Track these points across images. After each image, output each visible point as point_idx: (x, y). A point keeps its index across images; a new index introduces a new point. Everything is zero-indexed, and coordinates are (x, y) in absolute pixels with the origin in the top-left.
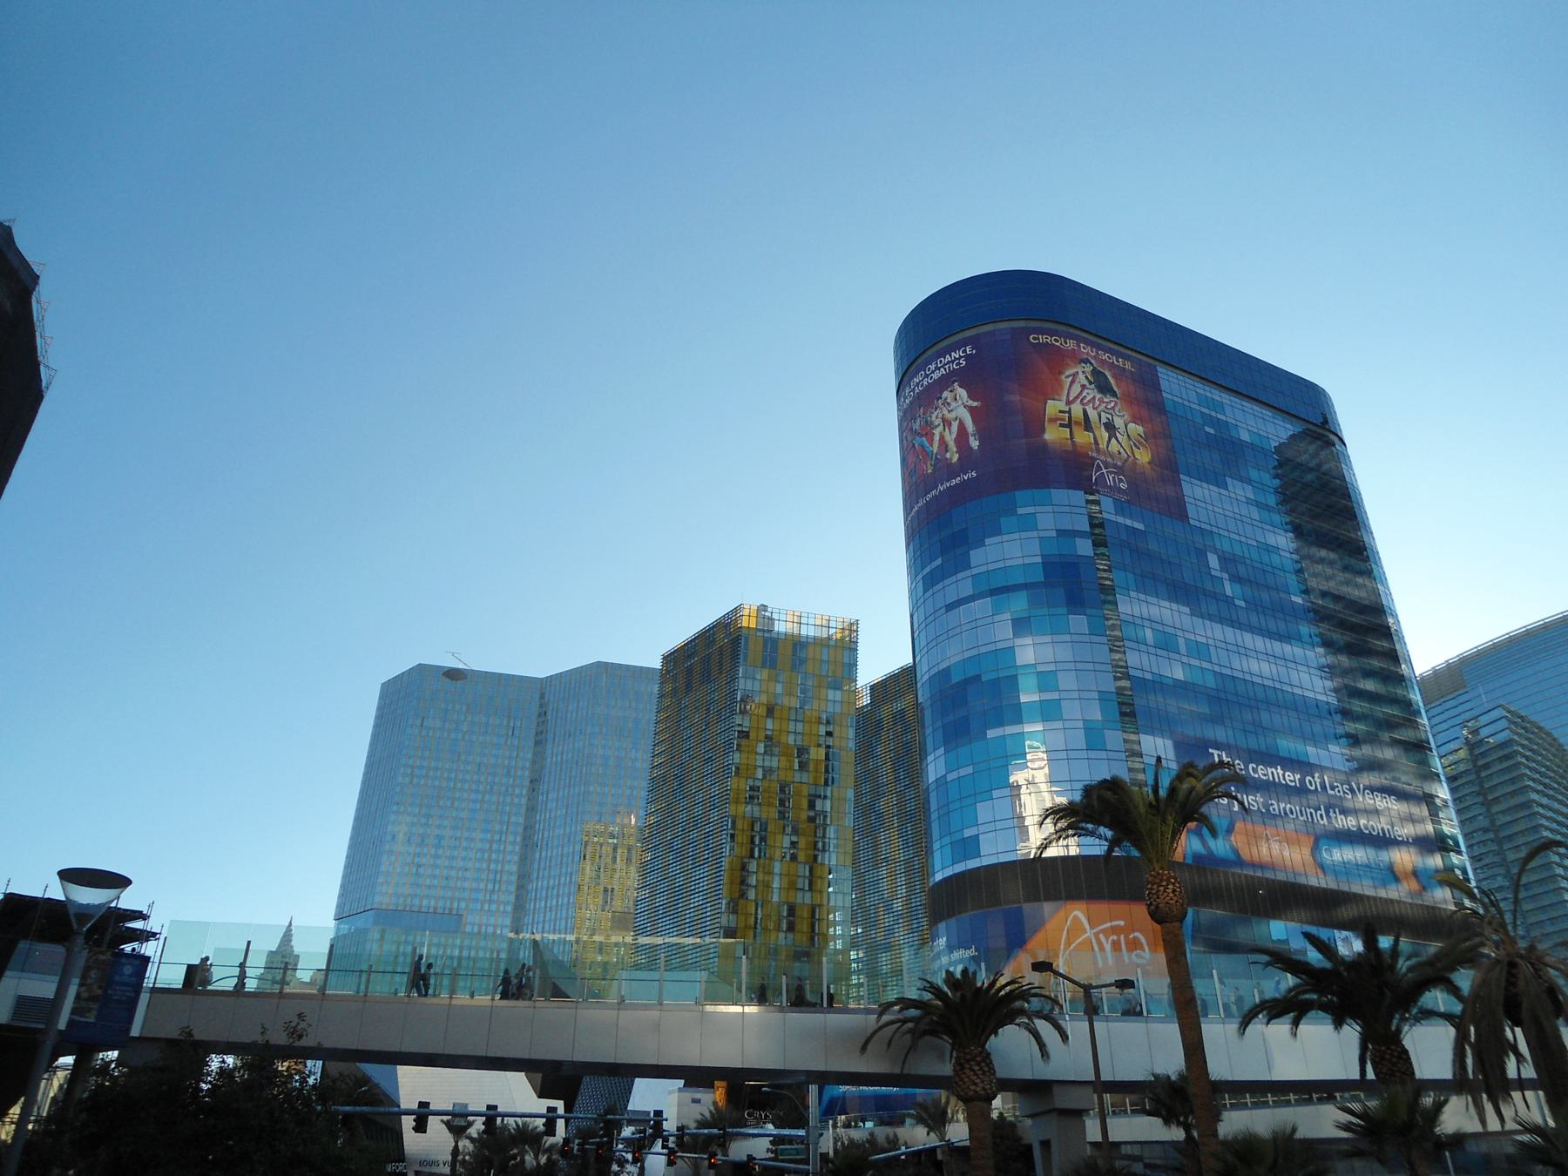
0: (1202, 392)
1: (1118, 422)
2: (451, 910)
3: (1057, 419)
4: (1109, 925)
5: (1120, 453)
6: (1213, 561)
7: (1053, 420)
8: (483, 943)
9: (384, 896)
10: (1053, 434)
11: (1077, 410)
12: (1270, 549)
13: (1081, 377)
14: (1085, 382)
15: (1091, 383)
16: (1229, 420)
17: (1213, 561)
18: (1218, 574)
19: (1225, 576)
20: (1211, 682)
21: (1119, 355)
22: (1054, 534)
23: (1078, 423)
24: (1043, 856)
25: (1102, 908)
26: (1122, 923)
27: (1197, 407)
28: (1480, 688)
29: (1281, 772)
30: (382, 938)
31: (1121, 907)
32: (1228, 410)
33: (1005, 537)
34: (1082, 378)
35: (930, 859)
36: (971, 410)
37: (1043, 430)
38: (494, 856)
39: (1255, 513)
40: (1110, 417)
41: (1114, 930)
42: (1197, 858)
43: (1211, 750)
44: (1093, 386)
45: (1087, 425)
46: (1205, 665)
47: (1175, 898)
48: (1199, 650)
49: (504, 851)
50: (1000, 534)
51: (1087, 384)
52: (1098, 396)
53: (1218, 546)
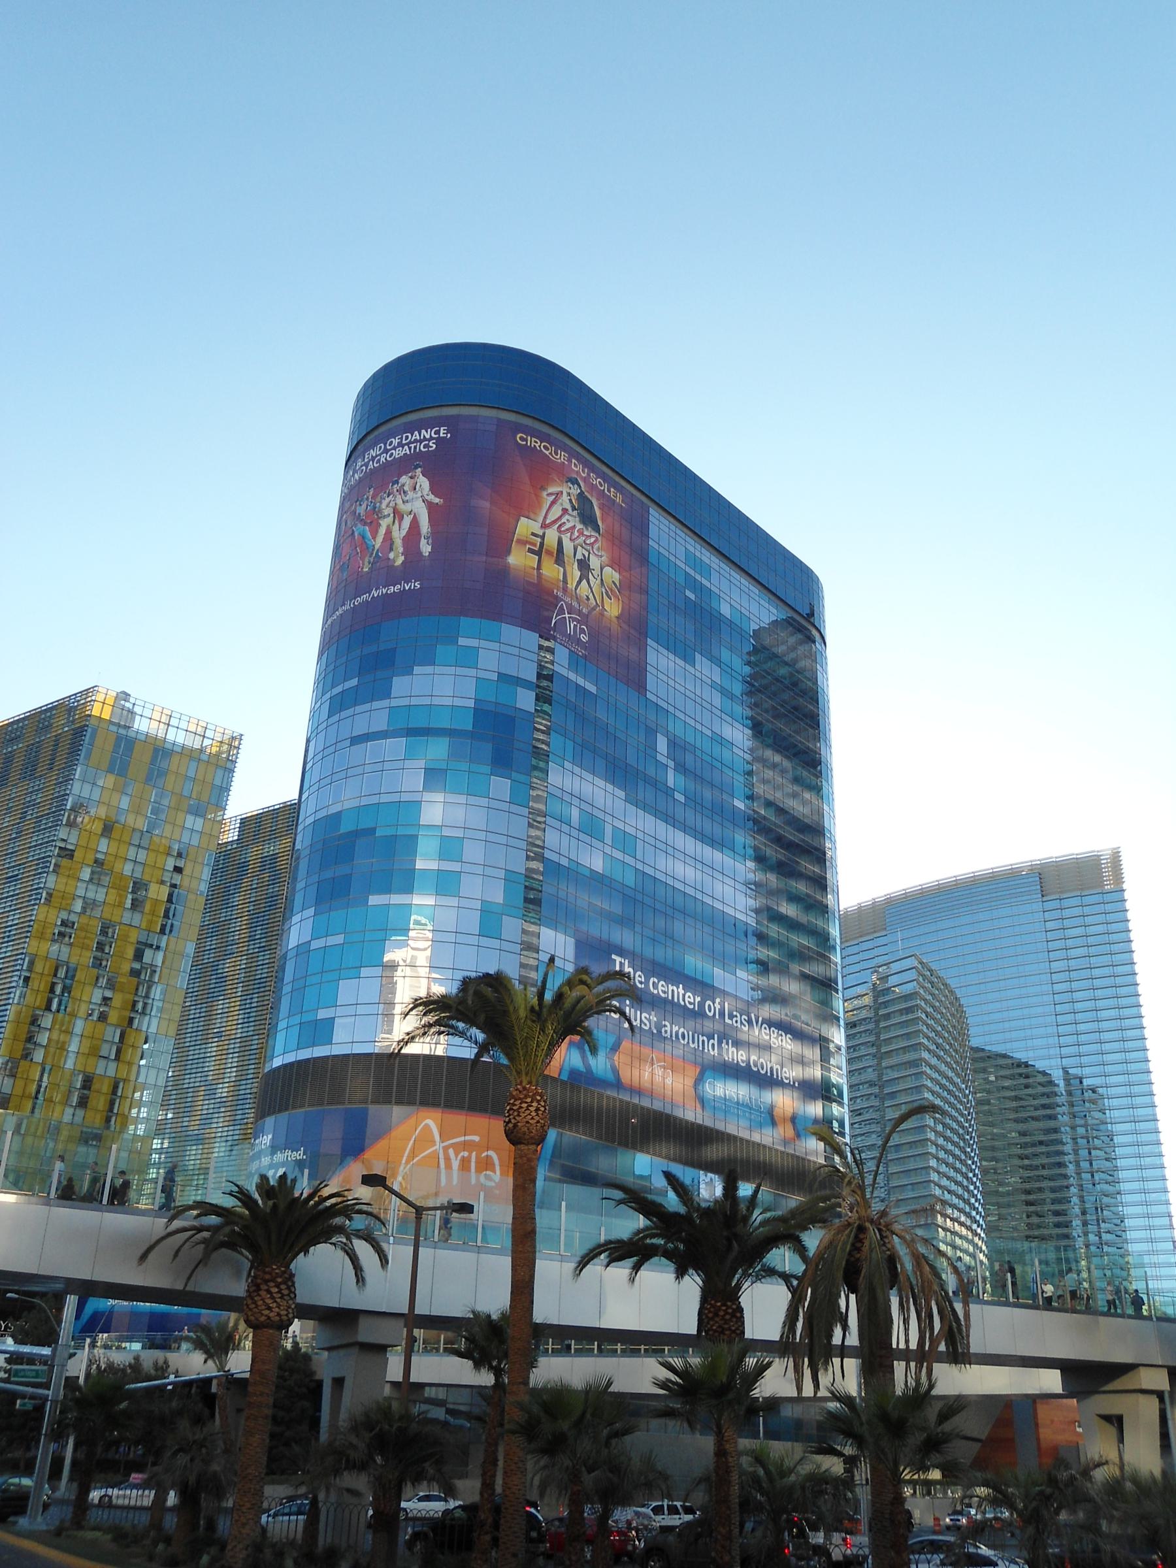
0: (692, 550)
1: (594, 563)
4: (462, 1139)
5: (588, 598)
6: (662, 744)
7: (522, 542)
10: (519, 559)
12: (721, 741)
13: (565, 498)
15: (574, 509)
16: (713, 588)
17: (662, 744)
18: (664, 760)
19: (671, 764)
20: (630, 880)
22: (495, 677)
25: (458, 1119)
26: (476, 1138)
27: (683, 566)
29: (681, 991)
32: (714, 576)
36: (430, 506)
37: (509, 552)
39: (717, 699)
40: (586, 554)
41: (466, 1145)
43: (614, 957)
44: (575, 513)
46: (629, 860)
47: (537, 1118)
48: (625, 841)
50: (432, 663)
51: (568, 507)
52: (579, 526)
53: (670, 728)
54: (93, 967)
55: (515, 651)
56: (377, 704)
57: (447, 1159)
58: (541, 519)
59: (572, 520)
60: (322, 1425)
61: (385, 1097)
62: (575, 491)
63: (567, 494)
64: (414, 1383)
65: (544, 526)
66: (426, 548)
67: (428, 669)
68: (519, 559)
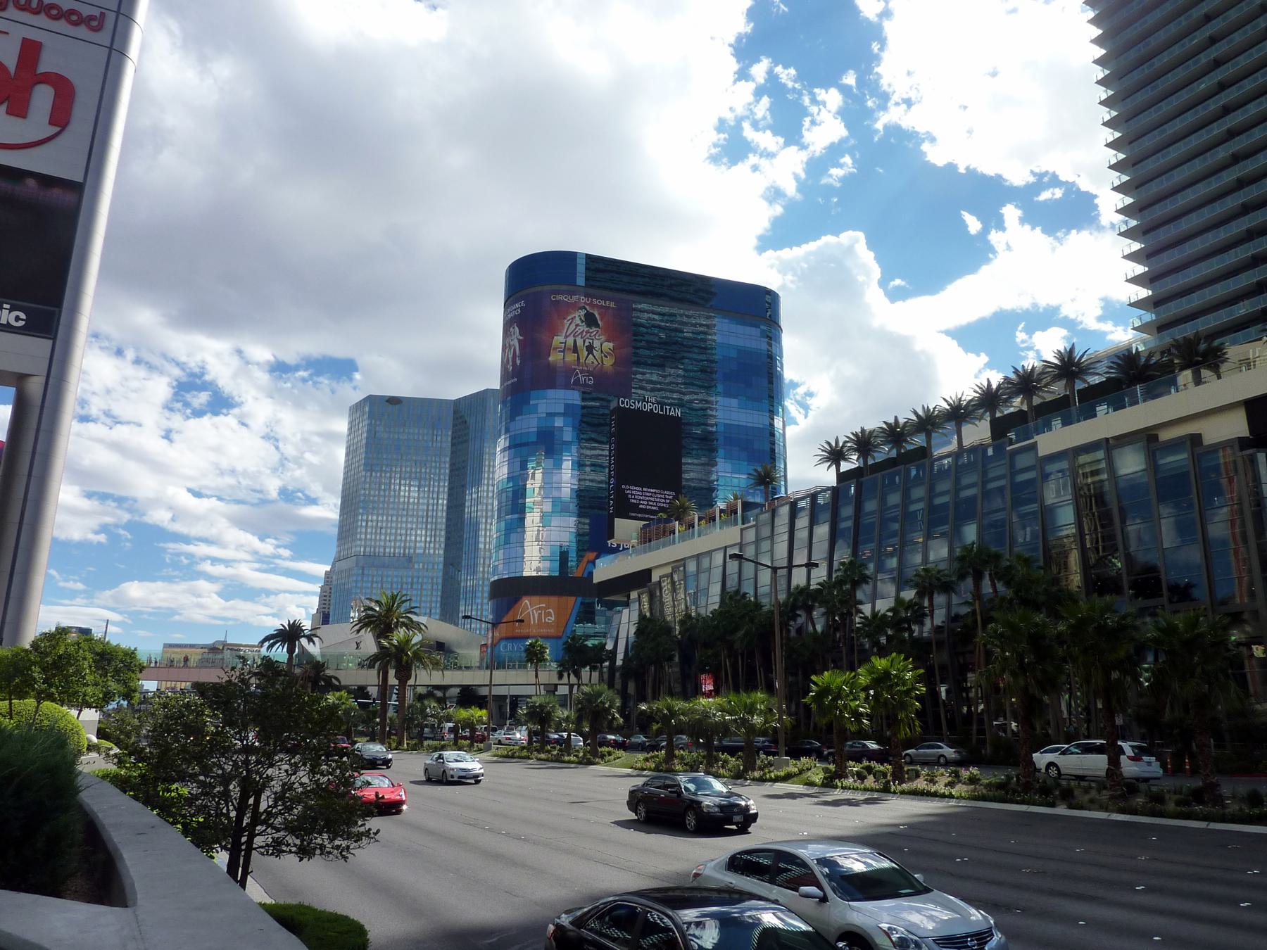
1: (597, 344)
7: (555, 349)
8: (426, 574)
10: (554, 357)
11: (570, 341)
13: (577, 319)
14: (579, 322)
15: (582, 322)
21: (605, 299)
22: (545, 415)
23: (569, 349)
25: (536, 599)
28: (1251, 357)
31: (545, 598)
33: (524, 417)
34: (577, 321)
36: (519, 340)
38: (410, 519)
40: (591, 341)
45: (575, 349)
49: (436, 517)
54: (114, 694)
55: (554, 401)
56: (532, 416)
59: (583, 328)
62: (583, 312)
65: (566, 337)
68: (554, 357)
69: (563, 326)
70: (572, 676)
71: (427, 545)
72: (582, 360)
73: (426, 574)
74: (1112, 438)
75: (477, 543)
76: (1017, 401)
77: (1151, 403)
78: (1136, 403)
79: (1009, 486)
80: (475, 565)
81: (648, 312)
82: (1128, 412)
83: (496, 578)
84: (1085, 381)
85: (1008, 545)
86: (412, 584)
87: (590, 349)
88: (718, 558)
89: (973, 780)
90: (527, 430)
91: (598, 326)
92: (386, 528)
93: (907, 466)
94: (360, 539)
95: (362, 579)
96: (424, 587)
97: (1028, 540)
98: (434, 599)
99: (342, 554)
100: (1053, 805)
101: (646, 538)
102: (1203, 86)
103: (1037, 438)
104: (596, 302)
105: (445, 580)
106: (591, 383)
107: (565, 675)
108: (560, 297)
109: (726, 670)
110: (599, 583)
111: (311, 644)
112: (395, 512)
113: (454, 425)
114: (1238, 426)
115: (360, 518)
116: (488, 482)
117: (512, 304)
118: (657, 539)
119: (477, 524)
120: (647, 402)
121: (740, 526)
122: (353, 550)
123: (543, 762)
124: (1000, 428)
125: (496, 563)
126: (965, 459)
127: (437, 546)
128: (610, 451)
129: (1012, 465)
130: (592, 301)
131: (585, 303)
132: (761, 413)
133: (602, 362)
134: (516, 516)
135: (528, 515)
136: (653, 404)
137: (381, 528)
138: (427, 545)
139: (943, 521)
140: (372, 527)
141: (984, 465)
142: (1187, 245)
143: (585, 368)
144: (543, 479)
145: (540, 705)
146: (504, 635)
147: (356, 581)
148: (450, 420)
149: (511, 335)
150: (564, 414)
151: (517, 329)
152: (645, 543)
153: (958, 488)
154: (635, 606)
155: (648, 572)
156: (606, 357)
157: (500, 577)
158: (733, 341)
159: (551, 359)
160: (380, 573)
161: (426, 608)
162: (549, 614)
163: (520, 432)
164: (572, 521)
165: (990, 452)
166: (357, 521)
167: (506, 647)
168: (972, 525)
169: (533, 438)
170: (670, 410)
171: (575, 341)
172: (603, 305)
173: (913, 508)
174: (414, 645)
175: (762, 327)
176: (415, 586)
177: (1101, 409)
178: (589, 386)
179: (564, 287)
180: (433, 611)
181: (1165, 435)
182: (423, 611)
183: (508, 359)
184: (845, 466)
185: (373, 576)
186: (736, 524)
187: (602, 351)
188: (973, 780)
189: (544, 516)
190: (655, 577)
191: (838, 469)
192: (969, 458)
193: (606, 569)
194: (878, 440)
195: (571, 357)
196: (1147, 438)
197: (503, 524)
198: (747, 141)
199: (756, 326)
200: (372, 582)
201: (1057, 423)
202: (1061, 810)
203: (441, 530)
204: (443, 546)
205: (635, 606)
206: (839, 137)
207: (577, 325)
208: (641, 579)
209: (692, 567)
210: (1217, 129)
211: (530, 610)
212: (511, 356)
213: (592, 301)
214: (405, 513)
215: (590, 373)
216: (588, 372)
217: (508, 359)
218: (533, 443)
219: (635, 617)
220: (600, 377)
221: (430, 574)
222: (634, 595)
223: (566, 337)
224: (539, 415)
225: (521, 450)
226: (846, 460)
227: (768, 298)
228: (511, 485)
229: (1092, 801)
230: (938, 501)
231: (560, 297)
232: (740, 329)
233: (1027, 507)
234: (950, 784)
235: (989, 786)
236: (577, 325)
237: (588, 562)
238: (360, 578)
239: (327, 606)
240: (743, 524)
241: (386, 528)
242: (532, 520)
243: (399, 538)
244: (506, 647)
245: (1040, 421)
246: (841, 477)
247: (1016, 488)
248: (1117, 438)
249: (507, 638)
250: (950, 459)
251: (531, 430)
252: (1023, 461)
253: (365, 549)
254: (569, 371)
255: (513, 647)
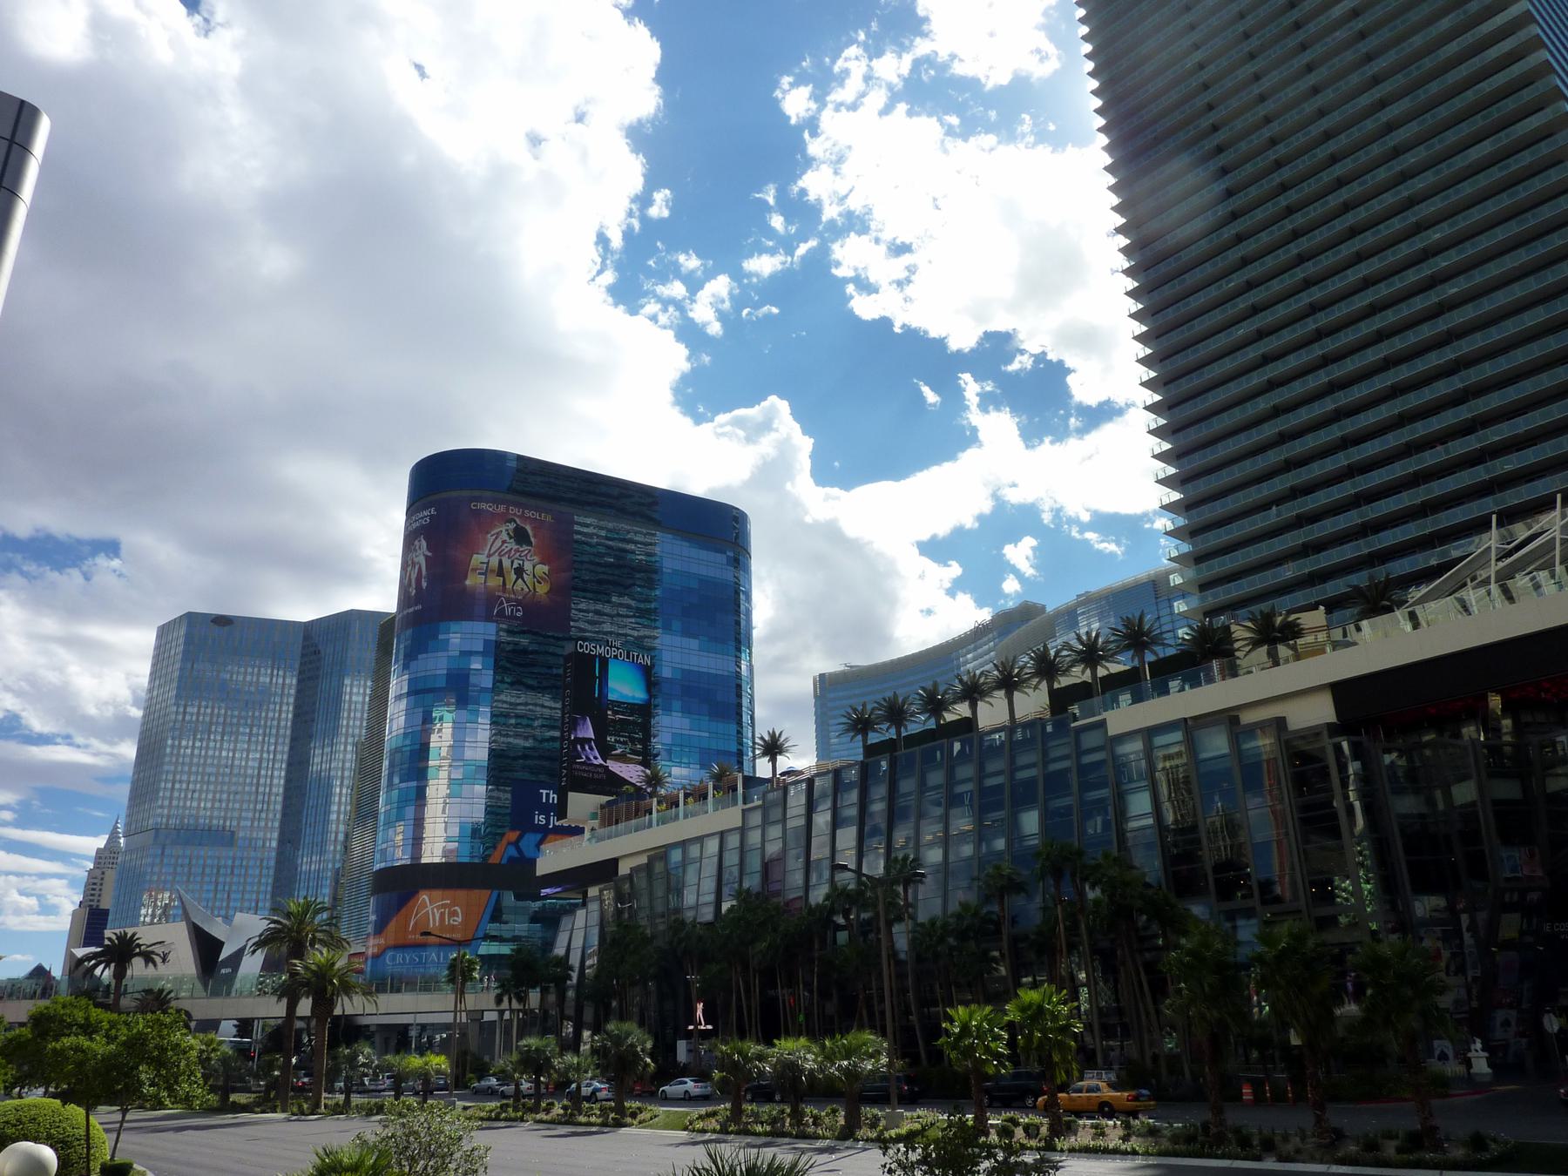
1: (528, 566)
2: (224, 827)
3: (476, 570)
5: (522, 589)
7: (474, 570)
8: (253, 854)
9: (161, 813)
10: (473, 581)
11: (494, 561)
15: (511, 538)
22: (457, 653)
23: (492, 571)
24: (518, 833)
25: (437, 893)
30: (163, 853)
33: (430, 655)
34: (504, 536)
35: (977, 664)
36: (427, 558)
37: (466, 577)
41: (443, 906)
42: (1012, 726)
44: (512, 540)
45: (500, 572)
50: (427, 652)
51: (507, 539)
56: (440, 654)
57: (433, 914)
58: (486, 552)
59: (512, 545)
60: (1350, 1172)
61: (925, 785)
62: (512, 526)
63: (504, 530)
64: (312, 1012)
65: (489, 556)
66: (424, 584)
67: (424, 655)
68: (473, 581)
69: (485, 540)
70: (514, 1001)
71: (257, 815)
72: (509, 586)
73: (253, 854)
74: (1191, 718)
75: (327, 812)
76: (1077, 670)
77: (1231, 682)
78: (1210, 680)
79: (1074, 770)
80: (323, 843)
81: (590, 526)
82: (1206, 689)
83: (383, 865)
84: (1155, 653)
85: (1076, 837)
86: (233, 867)
87: (519, 572)
88: (712, 846)
89: (1152, 1132)
90: (433, 672)
91: (530, 544)
92: (201, 791)
93: (950, 740)
94: (162, 807)
95: (162, 861)
96: (250, 872)
97: (1099, 831)
98: (263, 888)
99: (133, 826)
100: (1258, 1159)
101: (610, 817)
102: (1241, 331)
103: (1105, 715)
104: (528, 514)
105: (278, 862)
106: (519, 614)
107: (506, 999)
108: (484, 506)
109: (738, 992)
110: (543, 876)
111: (151, 965)
112: (234, 780)
113: (303, 655)
114: (1321, 711)
115: (164, 777)
116: (347, 731)
117: (418, 511)
118: (628, 819)
119: (330, 786)
120: (611, 647)
121: (741, 805)
122: (151, 821)
123: (553, 1126)
124: (1060, 700)
125: (384, 846)
126: (1019, 735)
127: (271, 816)
128: (564, 706)
129: (1078, 743)
130: (523, 512)
131: (515, 514)
132: (725, 657)
133: (534, 589)
134: (414, 784)
135: (431, 782)
136: (618, 649)
137: (194, 791)
138: (257, 815)
139: (998, 806)
140: (180, 790)
141: (1044, 743)
142: (1229, 499)
143: (513, 596)
144: (453, 735)
145: (537, 1049)
146: (391, 942)
147: (153, 865)
148: (298, 649)
149: (415, 550)
150: (484, 654)
151: (424, 543)
152: (610, 824)
153: (1013, 769)
154: (594, 907)
155: (613, 863)
156: (540, 583)
157: (389, 864)
158: (694, 569)
159: (468, 582)
160: (188, 852)
161: (250, 901)
162: (454, 914)
163: (423, 674)
164: (481, 789)
165: (1049, 729)
166: (160, 781)
167: (393, 958)
168: (1032, 812)
169: (442, 683)
170: (638, 656)
171: (500, 562)
172: (531, 517)
173: (960, 789)
174: (339, 970)
175: (728, 553)
176: (236, 871)
177: (1174, 684)
178: (516, 618)
179: (488, 494)
180: (260, 905)
181: (1248, 718)
182: (246, 904)
183: (410, 580)
184: (874, 738)
185: (178, 857)
186: (735, 803)
187: (534, 576)
188: (1152, 1132)
189: (452, 782)
190: (624, 869)
191: (865, 740)
192: (1024, 733)
193: (554, 858)
194: (913, 708)
195: (494, 582)
196: (1229, 718)
197: (395, 793)
198: (697, 325)
199: (723, 552)
200: (176, 866)
201: (1125, 698)
202: (1270, 1164)
203: (278, 795)
204: (278, 816)
205: (594, 907)
206: (705, 289)
207: (504, 542)
208: (604, 871)
209: (676, 856)
210: (1256, 379)
211: (429, 908)
212: (414, 576)
213: (523, 512)
214: (228, 770)
215: (519, 603)
216: (516, 601)
217: (410, 580)
218: (440, 689)
219: (595, 918)
220: (531, 608)
221: (259, 855)
222: (593, 891)
223: (489, 556)
224: (451, 653)
225: (423, 695)
226: (875, 731)
227: (736, 519)
228: (408, 742)
229: (1298, 1151)
230: (990, 782)
231: (484, 506)
232: (704, 554)
233: (1097, 792)
234: (1125, 1139)
235: (1175, 1139)
236: (504, 542)
237: (509, 843)
238: (158, 861)
239: (96, 898)
240: (745, 803)
241: (201, 791)
242: (437, 789)
243: (217, 805)
244: (393, 958)
245: (1108, 695)
246: (870, 750)
247: (1083, 770)
248: (1195, 718)
249: (396, 947)
250: (1003, 734)
251: (438, 672)
252: (1090, 740)
253: (168, 820)
254: (492, 599)
255: (404, 959)
